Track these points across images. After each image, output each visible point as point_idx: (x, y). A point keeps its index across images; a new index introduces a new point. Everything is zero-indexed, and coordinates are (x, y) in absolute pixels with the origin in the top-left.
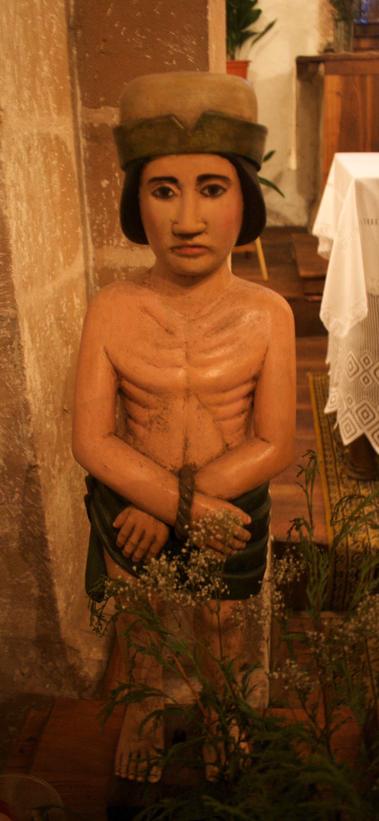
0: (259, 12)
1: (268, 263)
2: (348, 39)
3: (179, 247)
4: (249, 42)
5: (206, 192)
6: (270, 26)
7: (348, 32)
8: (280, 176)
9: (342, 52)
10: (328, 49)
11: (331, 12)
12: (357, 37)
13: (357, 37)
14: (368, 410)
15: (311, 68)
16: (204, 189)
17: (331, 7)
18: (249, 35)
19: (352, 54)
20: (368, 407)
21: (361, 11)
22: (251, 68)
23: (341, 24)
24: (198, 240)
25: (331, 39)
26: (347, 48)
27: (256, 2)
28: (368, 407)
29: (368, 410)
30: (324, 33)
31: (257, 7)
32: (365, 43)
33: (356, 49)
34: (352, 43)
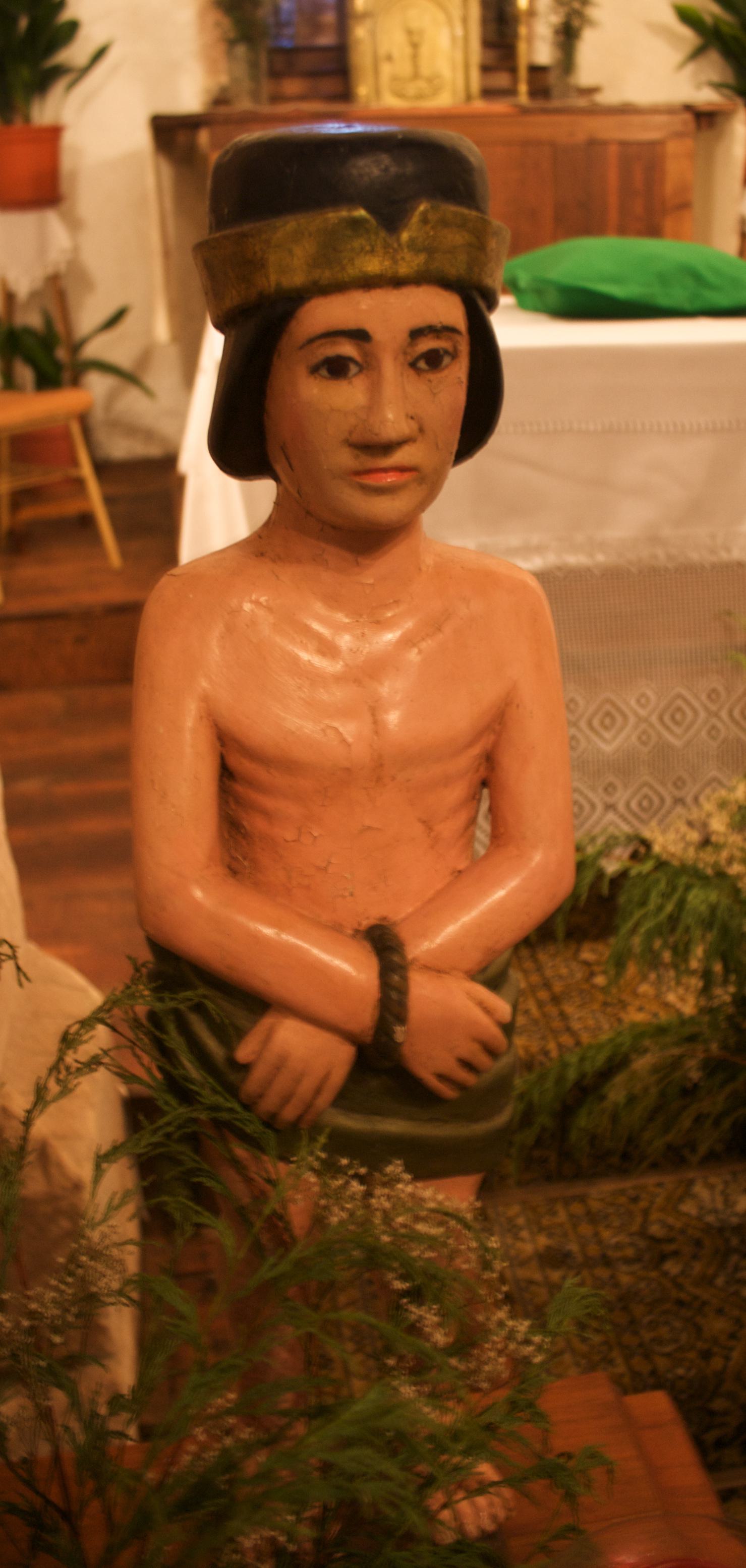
0: (73, 27)
1: (122, 532)
2: (255, 78)
3: (358, 473)
4: (59, 88)
5: (422, 364)
6: (100, 54)
7: (253, 65)
8: (146, 357)
9: (244, 104)
10: (220, 100)
11: (217, 24)
12: (275, 74)
13: (275, 74)
14: (650, 793)
15: (181, 138)
16: (417, 359)
17: (215, 16)
18: (58, 71)
19: (266, 109)
20: (651, 787)
21: (280, 25)
22: (69, 139)
23: (241, 50)
24: (400, 457)
25: (224, 79)
26: (255, 96)
27: (61, 5)
28: (651, 787)
29: (650, 793)
30: (212, 68)
31: (67, 15)
32: (292, 86)
33: (276, 98)
34: (267, 87)
